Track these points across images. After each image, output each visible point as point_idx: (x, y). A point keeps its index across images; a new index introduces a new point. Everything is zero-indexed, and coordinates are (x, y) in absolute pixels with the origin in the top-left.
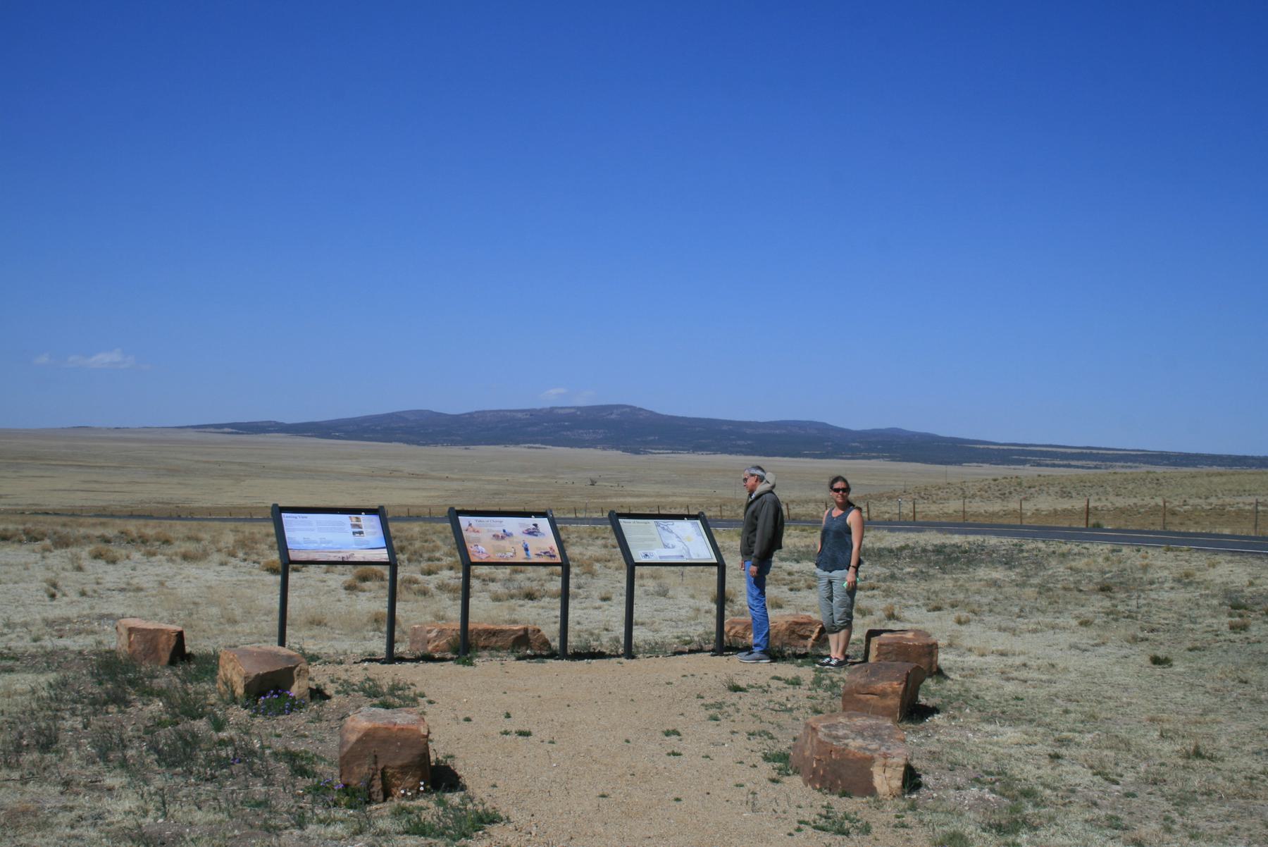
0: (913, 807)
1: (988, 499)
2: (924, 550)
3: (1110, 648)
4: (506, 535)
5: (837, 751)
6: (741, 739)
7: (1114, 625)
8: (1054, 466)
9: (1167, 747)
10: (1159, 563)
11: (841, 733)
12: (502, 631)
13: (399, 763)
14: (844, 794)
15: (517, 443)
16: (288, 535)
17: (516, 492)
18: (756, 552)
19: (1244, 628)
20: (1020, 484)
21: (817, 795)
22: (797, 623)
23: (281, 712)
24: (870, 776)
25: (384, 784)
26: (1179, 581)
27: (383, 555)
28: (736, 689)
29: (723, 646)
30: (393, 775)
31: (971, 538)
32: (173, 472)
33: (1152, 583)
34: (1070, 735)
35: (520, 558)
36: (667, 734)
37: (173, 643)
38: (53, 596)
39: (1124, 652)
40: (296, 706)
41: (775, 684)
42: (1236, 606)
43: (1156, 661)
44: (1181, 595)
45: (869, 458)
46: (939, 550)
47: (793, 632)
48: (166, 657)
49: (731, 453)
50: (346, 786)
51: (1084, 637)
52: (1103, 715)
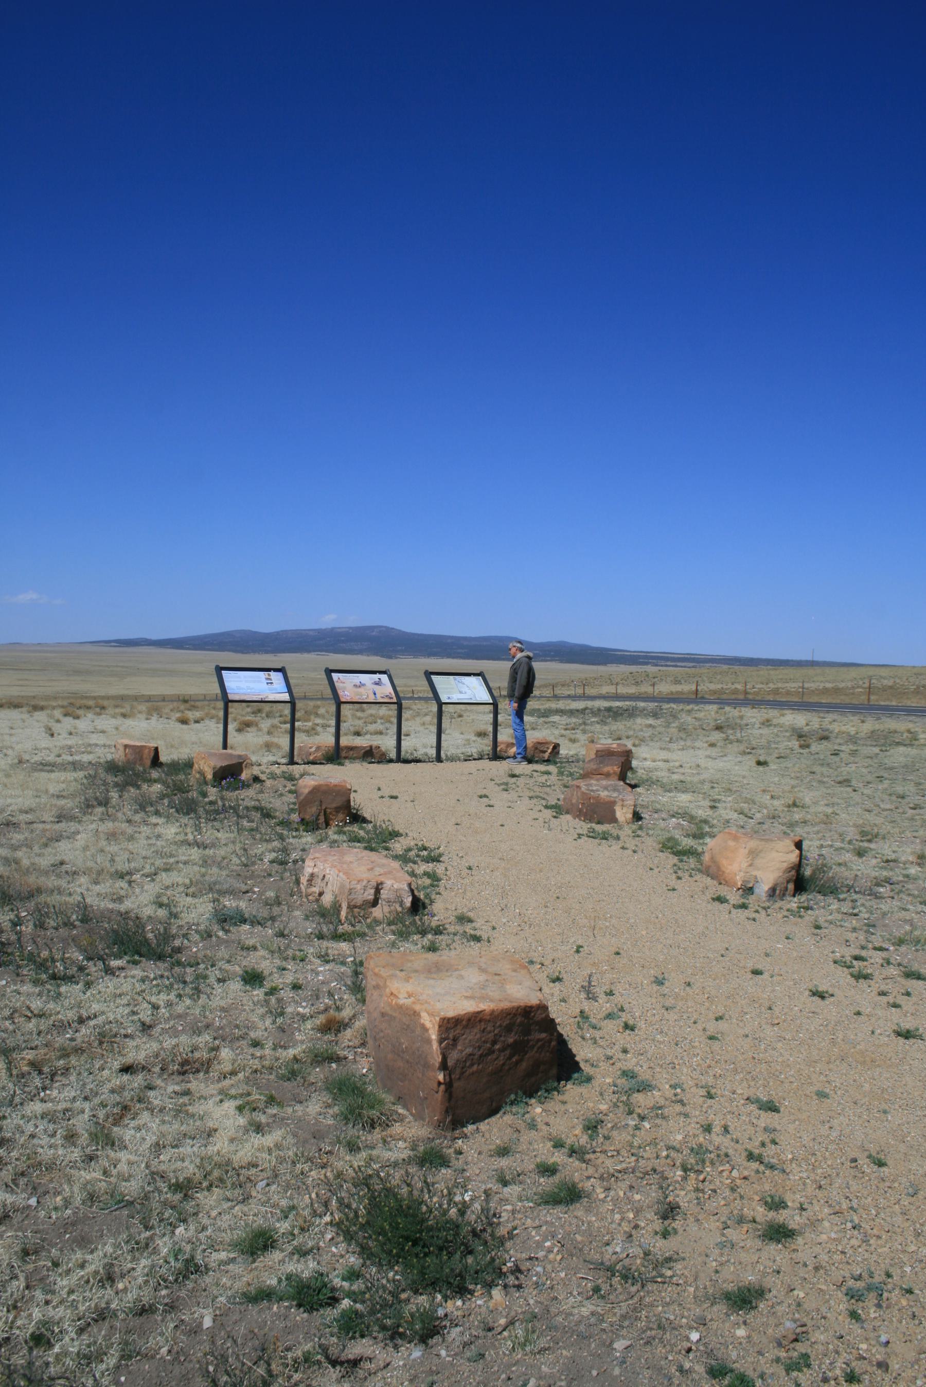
0: (641, 828)
1: (628, 685)
2: (599, 710)
3: (730, 758)
4: (362, 685)
5: (594, 798)
6: (526, 801)
7: (730, 746)
8: (667, 666)
9: (776, 803)
10: (749, 715)
11: (594, 788)
12: (356, 747)
13: (334, 805)
14: (598, 823)
15: (309, 651)
16: (227, 684)
17: (310, 684)
18: (516, 694)
19: (808, 746)
20: (647, 676)
21: (583, 823)
22: (539, 743)
23: (237, 789)
24: (614, 812)
25: (325, 818)
26: (763, 724)
27: (286, 697)
28: (513, 776)
29: (496, 756)
30: (331, 813)
31: (627, 703)
32: (77, 672)
33: (747, 725)
34: (719, 797)
35: (371, 699)
36: (481, 797)
37: (152, 754)
38: (52, 735)
39: (739, 759)
40: (245, 785)
41: (535, 774)
42: (800, 736)
43: (759, 763)
44: (765, 731)
45: (546, 661)
46: (609, 709)
47: (536, 748)
48: (148, 762)
49: (453, 658)
50: (302, 820)
51: (713, 752)
52: (735, 789)
